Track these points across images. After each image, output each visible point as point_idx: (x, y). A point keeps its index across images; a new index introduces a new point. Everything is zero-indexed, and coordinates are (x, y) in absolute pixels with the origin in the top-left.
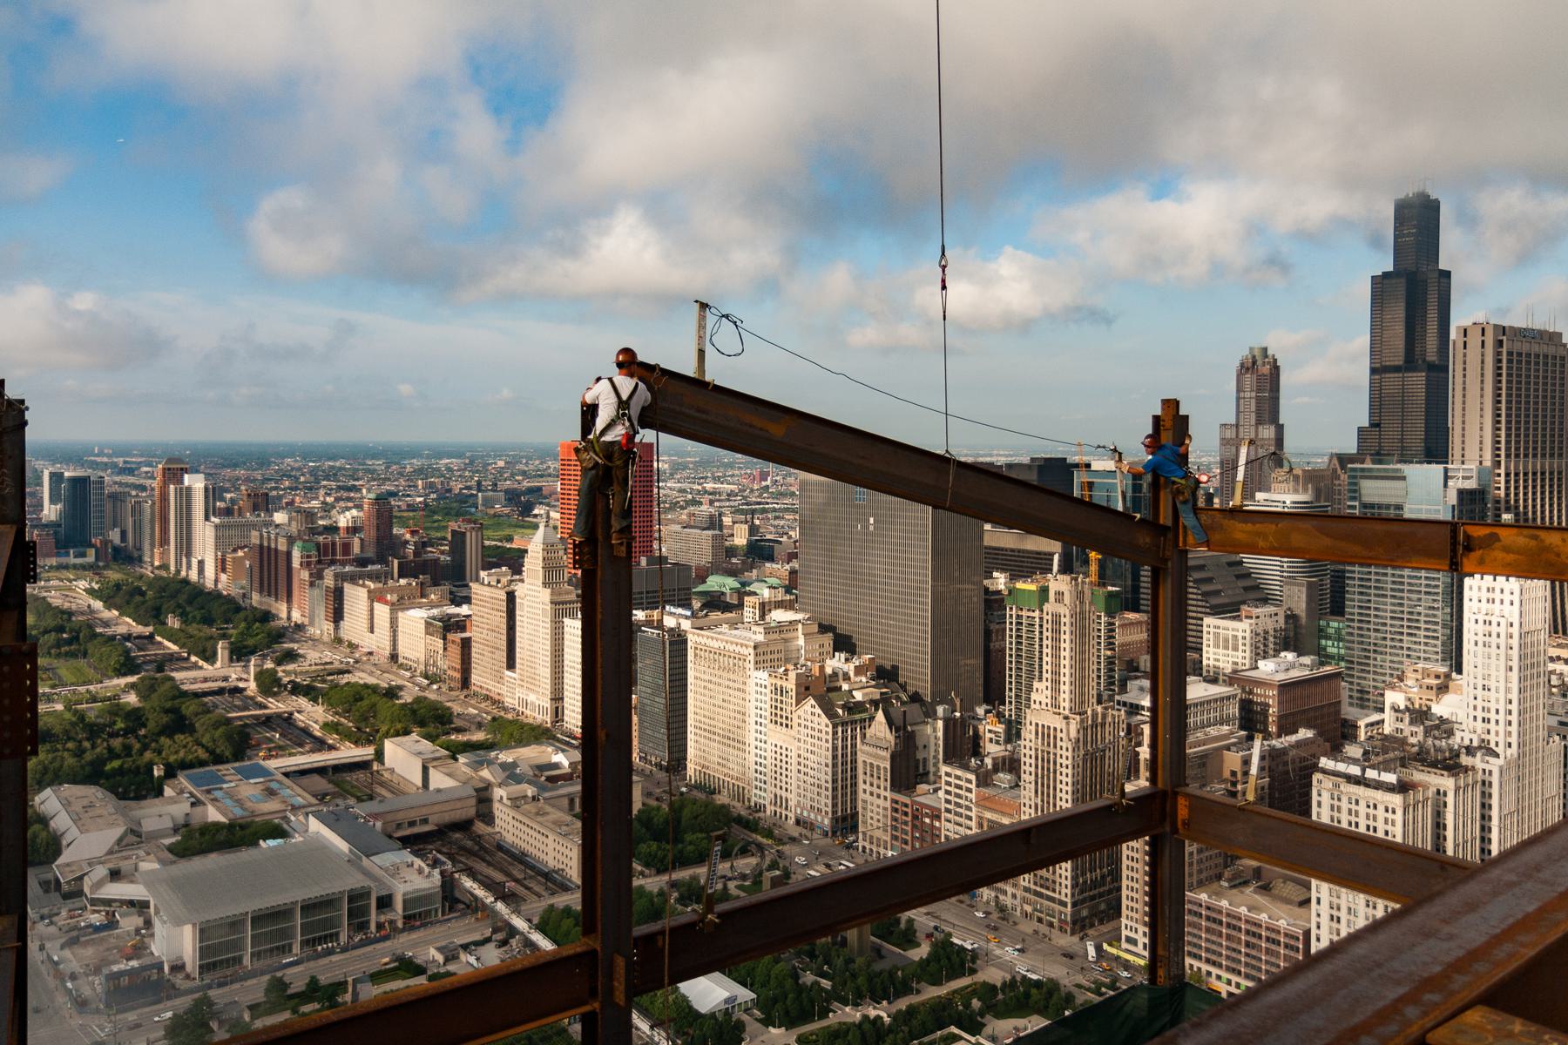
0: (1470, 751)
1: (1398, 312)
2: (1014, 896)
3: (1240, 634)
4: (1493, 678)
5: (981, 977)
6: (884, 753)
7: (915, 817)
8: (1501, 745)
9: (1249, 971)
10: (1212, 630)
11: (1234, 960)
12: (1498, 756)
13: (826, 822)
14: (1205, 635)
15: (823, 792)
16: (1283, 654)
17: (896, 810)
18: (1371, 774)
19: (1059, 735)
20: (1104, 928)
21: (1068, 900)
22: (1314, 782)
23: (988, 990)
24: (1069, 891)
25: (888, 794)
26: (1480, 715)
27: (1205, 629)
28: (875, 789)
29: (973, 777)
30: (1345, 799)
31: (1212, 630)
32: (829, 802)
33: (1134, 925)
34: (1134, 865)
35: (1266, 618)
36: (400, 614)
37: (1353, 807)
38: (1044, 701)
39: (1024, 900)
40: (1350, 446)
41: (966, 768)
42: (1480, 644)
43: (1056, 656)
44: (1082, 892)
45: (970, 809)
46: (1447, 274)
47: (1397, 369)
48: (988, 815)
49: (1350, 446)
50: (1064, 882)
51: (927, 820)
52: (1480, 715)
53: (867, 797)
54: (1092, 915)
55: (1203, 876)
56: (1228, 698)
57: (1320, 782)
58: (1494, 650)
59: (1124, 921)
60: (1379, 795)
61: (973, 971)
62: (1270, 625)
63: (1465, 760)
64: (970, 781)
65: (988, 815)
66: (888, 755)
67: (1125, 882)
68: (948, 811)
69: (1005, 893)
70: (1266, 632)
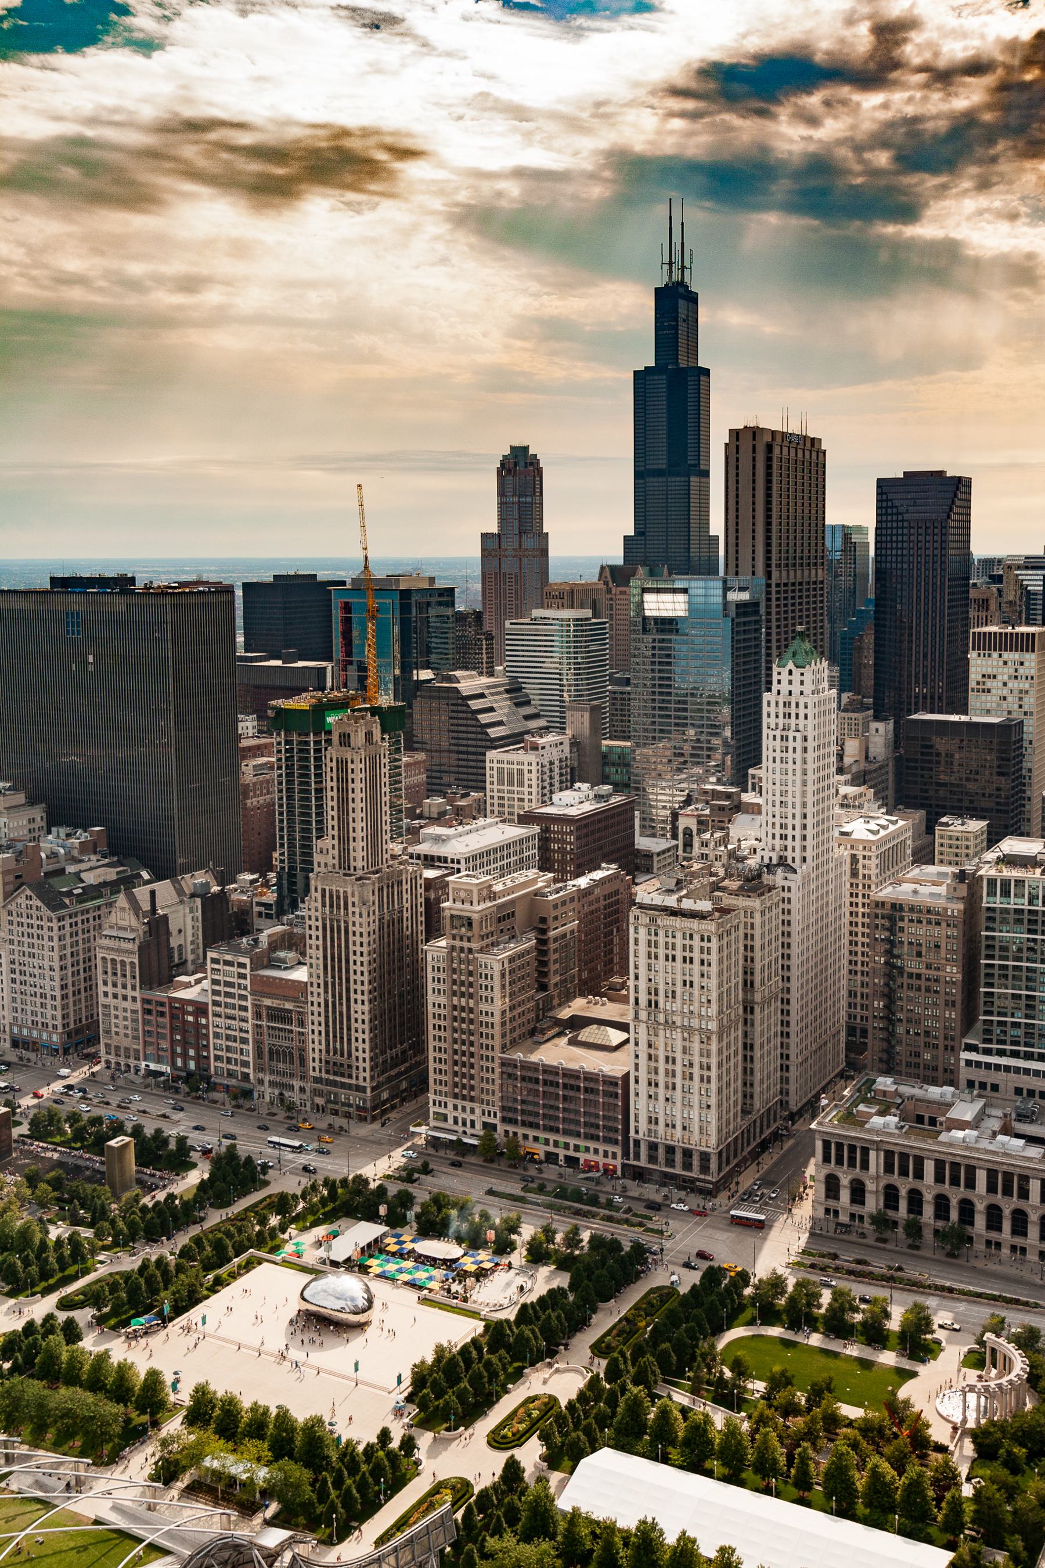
0: (770, 868)
1: (660, 406)
2: (302, 1090)
3: (526, 768)
4: (790, 794)
5: (274, 1189)
6: (129, 946)
7: (173, 1017)
8: (798, 860)
9: (547, 1122)
10: (495, 765)
11: (550, 1117)
12: (795, 871)
13: (55, 1038)
14: (488, 772)
15: (49, 1002)
16: (577, 785)
17: (149, 1012)
18: (687, 904)
19: (350, 900)
20: (409, 1107)
21: (367, 1084)
22: (632, 920)
23: (282, 1204)
24: (367, 1075)
25: (137, 994)
26: (778, 831)
27: (488, 765)
28: (119, 990)
29: (246, 961)
30: (661, 933)
31: (495, 765)
32: (59, 1013)
33: (443, 1099)
34: (442, 1034)
35: (553, 745)
36: (556, 576)
37: (688, 942)
38: (331, 862)
39: (316, 1093)
40: (616, 555)
41: (238, 950)
42: (778, 760)
43: (343, 802)
44: (383, 1072)
45: (243, 998)
46: (706, 372)
47: (660, 473)
48: (268, 1002)
49: (616, 555)
50: (361, 1064)
51: (190, 1019)
52: (778, 831)
53: (110, 1000)
54: (392, 1097)
55: (515, 1035)
56: (528, 839)
57: (637, 918)
58: (790, 766)
59: (431, 1096)
60: (694, 924)
61: (266, 1183)
62: (555, 755)
63: (767, 879)
64: (242, 965)
65: (268, 1002)
66: (133, 947)
67: (431, 1054)
68: (216, 1003)
69: (291, 1088)
70: (551, 763)
